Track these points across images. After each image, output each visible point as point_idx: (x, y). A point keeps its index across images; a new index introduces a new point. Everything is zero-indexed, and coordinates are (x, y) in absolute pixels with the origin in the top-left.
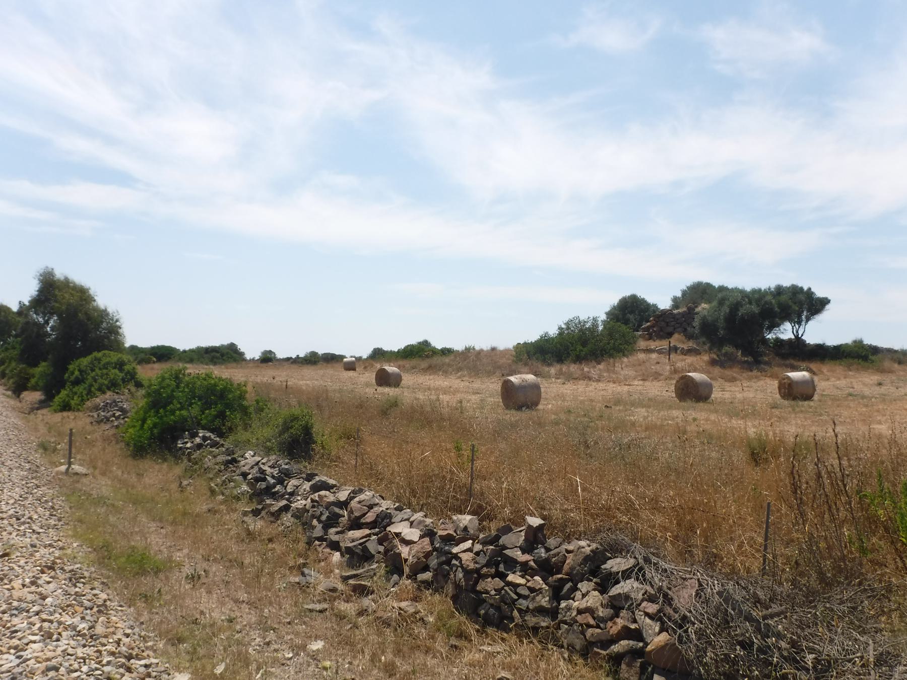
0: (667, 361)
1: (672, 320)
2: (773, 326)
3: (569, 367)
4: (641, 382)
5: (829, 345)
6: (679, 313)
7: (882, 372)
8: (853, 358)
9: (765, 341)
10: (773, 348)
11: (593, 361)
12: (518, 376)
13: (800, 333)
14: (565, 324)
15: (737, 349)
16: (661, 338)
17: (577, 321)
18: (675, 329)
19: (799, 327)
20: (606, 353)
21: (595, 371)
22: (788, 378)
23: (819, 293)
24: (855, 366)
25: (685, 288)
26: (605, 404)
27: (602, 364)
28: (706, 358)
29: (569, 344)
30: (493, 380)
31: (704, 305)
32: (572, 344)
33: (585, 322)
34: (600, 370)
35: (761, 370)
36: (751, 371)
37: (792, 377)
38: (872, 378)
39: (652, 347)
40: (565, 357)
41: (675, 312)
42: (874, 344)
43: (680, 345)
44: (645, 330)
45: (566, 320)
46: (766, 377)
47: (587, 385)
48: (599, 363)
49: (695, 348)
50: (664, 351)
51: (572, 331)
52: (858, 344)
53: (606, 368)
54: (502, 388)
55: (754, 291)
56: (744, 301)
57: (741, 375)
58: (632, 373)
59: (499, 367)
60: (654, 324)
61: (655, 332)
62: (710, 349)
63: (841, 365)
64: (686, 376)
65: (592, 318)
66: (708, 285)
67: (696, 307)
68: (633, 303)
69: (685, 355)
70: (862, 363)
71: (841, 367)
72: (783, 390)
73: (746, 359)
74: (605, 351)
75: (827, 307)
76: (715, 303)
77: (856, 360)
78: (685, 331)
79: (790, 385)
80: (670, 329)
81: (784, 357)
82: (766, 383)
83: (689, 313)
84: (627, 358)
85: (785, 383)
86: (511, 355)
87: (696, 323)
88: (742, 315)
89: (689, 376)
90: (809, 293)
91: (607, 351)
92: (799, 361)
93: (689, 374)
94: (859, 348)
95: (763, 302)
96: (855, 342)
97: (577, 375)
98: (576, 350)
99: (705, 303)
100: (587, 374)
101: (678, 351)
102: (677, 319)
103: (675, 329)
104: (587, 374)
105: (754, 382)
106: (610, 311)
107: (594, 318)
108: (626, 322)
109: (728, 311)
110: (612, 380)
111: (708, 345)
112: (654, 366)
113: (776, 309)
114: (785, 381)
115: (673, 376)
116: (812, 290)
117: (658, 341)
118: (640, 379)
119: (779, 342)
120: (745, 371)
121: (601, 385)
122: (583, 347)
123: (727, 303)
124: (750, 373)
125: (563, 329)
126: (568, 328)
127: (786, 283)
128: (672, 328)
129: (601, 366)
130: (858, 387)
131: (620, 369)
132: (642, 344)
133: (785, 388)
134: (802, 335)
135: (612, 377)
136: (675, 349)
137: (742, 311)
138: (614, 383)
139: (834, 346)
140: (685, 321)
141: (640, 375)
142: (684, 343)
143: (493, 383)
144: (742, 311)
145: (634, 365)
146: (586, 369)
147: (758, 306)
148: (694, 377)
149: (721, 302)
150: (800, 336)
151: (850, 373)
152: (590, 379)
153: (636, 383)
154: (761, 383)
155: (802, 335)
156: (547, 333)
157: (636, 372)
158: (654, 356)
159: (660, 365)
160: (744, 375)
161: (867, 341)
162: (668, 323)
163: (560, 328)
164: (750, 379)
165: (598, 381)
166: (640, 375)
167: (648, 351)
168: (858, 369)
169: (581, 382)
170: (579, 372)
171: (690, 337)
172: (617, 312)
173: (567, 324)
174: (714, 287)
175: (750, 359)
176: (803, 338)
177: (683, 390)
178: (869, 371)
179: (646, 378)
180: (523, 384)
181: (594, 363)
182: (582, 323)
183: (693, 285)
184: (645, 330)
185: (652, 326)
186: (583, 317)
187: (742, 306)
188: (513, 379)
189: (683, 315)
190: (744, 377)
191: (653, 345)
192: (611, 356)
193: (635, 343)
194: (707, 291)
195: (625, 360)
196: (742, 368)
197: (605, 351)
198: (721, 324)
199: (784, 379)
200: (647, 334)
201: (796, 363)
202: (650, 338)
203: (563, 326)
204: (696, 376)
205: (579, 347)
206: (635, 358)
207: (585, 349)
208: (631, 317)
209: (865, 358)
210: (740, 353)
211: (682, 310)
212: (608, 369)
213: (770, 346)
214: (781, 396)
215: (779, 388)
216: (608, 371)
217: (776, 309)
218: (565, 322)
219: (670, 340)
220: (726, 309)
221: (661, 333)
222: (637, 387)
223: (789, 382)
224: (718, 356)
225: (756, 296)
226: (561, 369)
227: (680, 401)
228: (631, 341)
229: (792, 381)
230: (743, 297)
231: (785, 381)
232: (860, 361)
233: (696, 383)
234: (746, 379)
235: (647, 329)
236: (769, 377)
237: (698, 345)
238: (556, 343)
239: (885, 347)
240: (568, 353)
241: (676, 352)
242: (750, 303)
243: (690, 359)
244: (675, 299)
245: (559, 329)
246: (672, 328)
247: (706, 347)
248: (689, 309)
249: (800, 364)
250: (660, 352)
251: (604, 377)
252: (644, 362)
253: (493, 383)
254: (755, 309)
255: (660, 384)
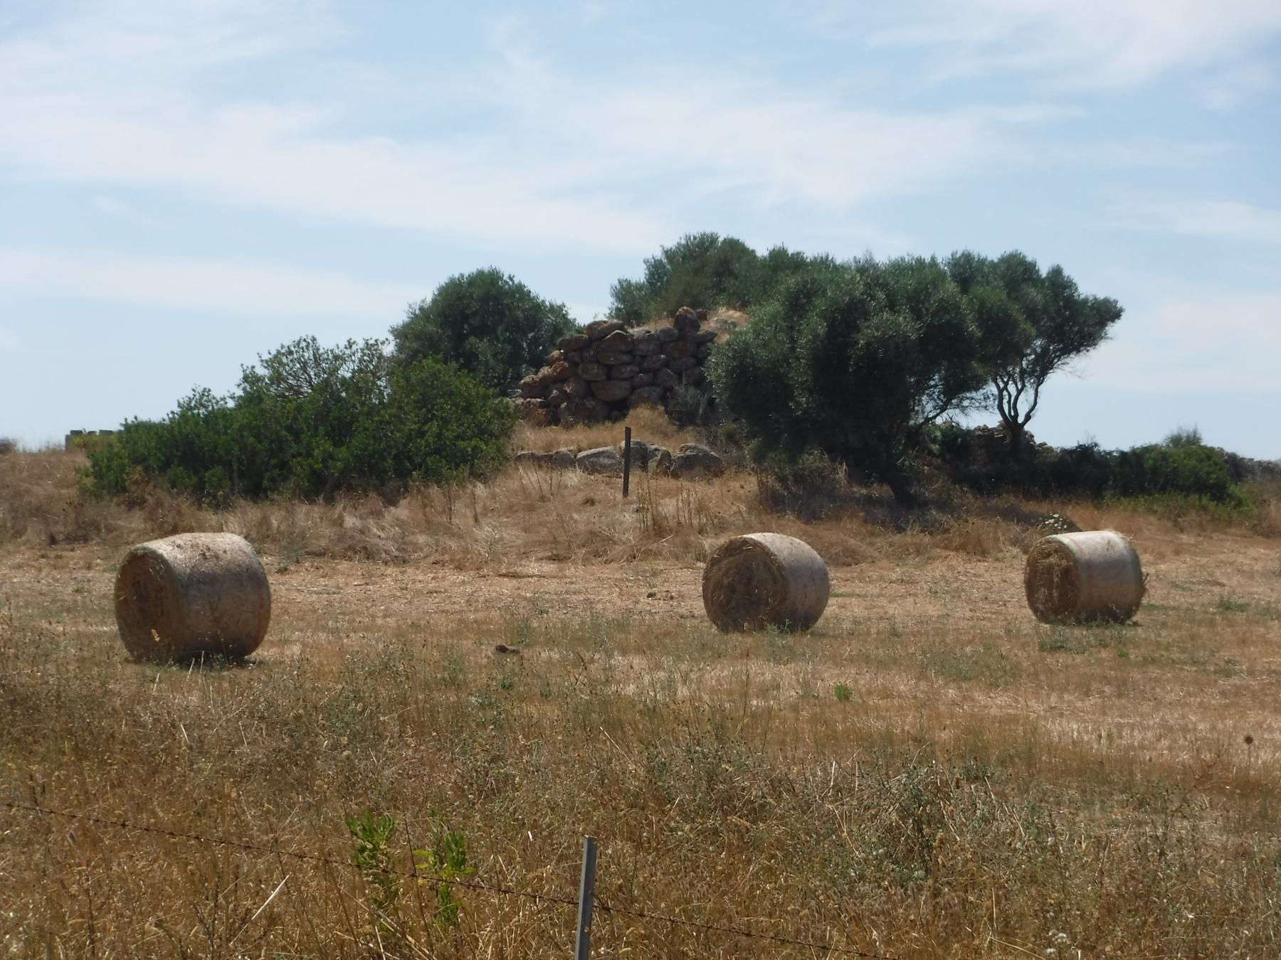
0: (619, 496)
1: (625, 358)
2: (955, 390)
3: (291, 513)
4: (550, 567)
5: (1209, 445)
6: (649, 338)
7: (1268, 537)
8: (1186, 490)
9: (917, 437)
10: (941, 456)
11: (372, 495)
12: (184, 538)
13: (1023, 409)
14: (268, 364)
15: (833, 460)
16: (590, 418)
17: (308, 355)
18: (633, 389)
19: (1019, 392)
20: (417, 467)
21: (383, 529)
22: (1062, 550)
23: (1089, 287)
24: (1193, 516)
25: (659, 254)
26: (499, 642)
27: (404, 502)
28: (749, 484)
29: (284, 432)
30: (18, 559)
31: (725, 313)
32: (297, 435)
33: (336, 358)
34: (399, 523)
35: (928, 528)
36: (900, 530)
37: (1073, 546)
38: (1253, 552)
39: (563, 449)
40: (273, 480)
41: (636, 331)
42: (1229, 448)
43: (656, 444)
44: (530, 390)
45: (270, 347)
46: (946, 548)
47: (368, 578)
48: (392, 501)
49: (706, 455)
50: (606, 461)
51: (291, 387)
52: (1187, 445)
53: (420, 515)
54: (121, 584)
55: (899, 269)
56: (873, 297)
57: (871, 544)
58: (512, 535)
59: (39, 512)
60: (564, 369)
61: (567, 397)
62: (759, 457)
63: (1151, 511)
64: (745, 542)
65: (361, 344)
66: (735, 248)
67: (703, 317)
68: (486, 298)
69: (675, 476)
70: (1212, 505)
71: (1152, 519)
72: (1042, 593)
73: (864, 491)
74: (409, 458)
75: (1112, 329)
76: (773, 307)
77: (1194, 498)
78: (665, 397)
79: (1066, 572)
80: (618, 390)
81: (984, 486)
82: (951, 568)
83: (682, 337)
84: (484, 483)
85: (1051, 567)
86: (78, 471)
87: (716, 369)
88: (868, 344)
89: (756, 544)
90: (1058, 283)
91: (418, 460)
92: (1045, 496)
93: (756, 536)
94: (1201, 461)
95: (933, 304)
96: (1176, 441)
97: (323, 543)
98: (309, 455)
99: (731, 306)
100: (358, 536)
101: (652, 464)
102: (644, 357)
103: (633, 389)
104: (358, 536)
105: (917, 567)
106: (406, 326)
107: (368, 346)
108: (468, 362)
109: (822, 329)
110: (447, 557)
111: (754, 443)
112: (579, 512)
113: (972, 328)
114: (1052, 560)
115: (654, 546)
116: (1067, 272)
117: (580, 427)
118: (540, 555)
119: (957, 441)
120: (878, 528)
121: (419, 577)
122: (335, 445)
123: (820, 304)
124: (897, 538)
125: (259, 379)
126: (277, 378)
127: (991, 250)
128: (626, 385)
129: (402, 511)
130: (1233, 585)
131: (471, 521)
132: (531, 438)
133: (1050, 585)
134: (1028, 417)
135: (445, 550)
136: (636, 457)
137: (867, 333)
138: (460, 568)
139: (1123, 454)
140: (666, 365)
141: (542, 543)
142: (665, 435)
143: (19, 567)
144: (867, 333)
145: (510, 509)
146: (351, 521)
147: (917, 314)
148: (773, 549)
149: (798, 304)
150: (1021, 420)
151: (1184, 538)
152: (369, 554)
153: (533, 567)
154: (937, 570)
155: (1028, 417)
156: (206, 392)
157: (526, 530)
158: (573, 477)
159: (598, 507)
160: (879, 541)
161: (1211, 439)
162: (610, 367)
163: (250, 378)
164: (899, 556)
165: (400, 561)
166: (542, 543)
167: (554, 461)
168: (1202, 527)
169: (344, 565)
170: (328, 531)
171: (684, 418)
172: (431, 328)
173: (275, 362)
174: (752, 253)
175: (880, 490)
176: (1027, 428)
177: (732, 589)
178: (1233, 530)
179: (562, 553)
180: (207, 567)
181: (375, 500)
182: (8, 440)
183: (687, 246)
184: (530, 390)
185: (560, 379)
186: (329, 342)
187: (866, 315)
188: (164, 547)
189: (661, 342)
190: (880, 550)
191: (568, 440)
192: (432, 476)
193: (506, 432)
194: (736, 266)
195: (480, 489)
196: (870, 520)
197: (409, 458)
198: (800, 373)
199: (1049, 555)
200: (542, 405)
201: (1029, 507)
202: (553, 418)
203: (261, 371)
204: (778, 544)
205: (323, 445)
206: (514, 484)
207: (343, 453)
208: (481, 346)
209: (1218, 492)
210: (841, 473)
211: (658, 325)
212: (428, 522)
213: (931, 452)
214: (1035, 611)
215: (1031, 586)
216: (429, 526)
217: (972, 328)
218: (266, 357)
219: (628, 422)
220: (815, 325)
221: (590, 404)
222: (544, 582)
223: (1064, 562)
224: (782, 479)
225: (911, 283)
226: (265, 521)
227: (725, 629)
228: (495, 427)
229: (1076, 561)
230: (867, 284)
231: (1052, 560)
232: (1205, 501)
233: (780, 568)
234: (887, 556)
235: (541, 388)
236: (957, 549)
237: (712, 444)
238: (241, 429)
239: (1257, 458)
240: (283, 465)
241: (644, 468)
242: (892, 305)
243: (699, 490)
244: (625, 292)
245: (246, 379)
246: (626, 385)
247: (748, 450)
248: (681, 322)
249: (1043, 508)
250: (592, 465)
251: (417, 548)
252: (543, 499)
253: (19, 567)
254: (906, 324)
255: (608, 572)
